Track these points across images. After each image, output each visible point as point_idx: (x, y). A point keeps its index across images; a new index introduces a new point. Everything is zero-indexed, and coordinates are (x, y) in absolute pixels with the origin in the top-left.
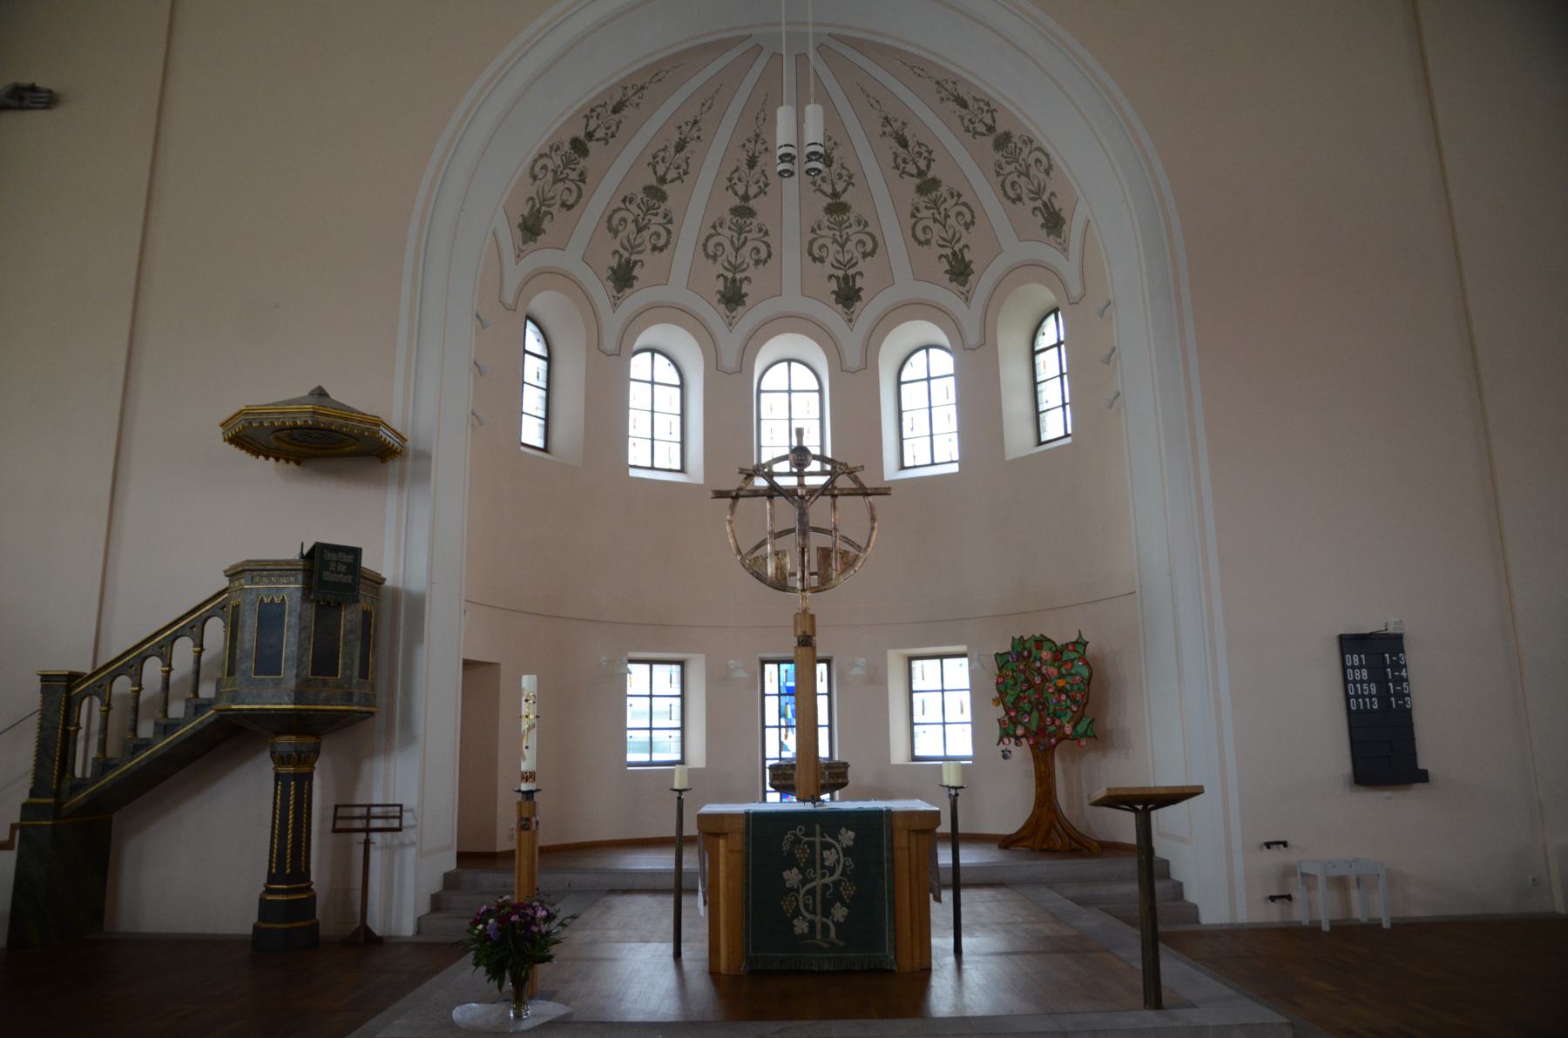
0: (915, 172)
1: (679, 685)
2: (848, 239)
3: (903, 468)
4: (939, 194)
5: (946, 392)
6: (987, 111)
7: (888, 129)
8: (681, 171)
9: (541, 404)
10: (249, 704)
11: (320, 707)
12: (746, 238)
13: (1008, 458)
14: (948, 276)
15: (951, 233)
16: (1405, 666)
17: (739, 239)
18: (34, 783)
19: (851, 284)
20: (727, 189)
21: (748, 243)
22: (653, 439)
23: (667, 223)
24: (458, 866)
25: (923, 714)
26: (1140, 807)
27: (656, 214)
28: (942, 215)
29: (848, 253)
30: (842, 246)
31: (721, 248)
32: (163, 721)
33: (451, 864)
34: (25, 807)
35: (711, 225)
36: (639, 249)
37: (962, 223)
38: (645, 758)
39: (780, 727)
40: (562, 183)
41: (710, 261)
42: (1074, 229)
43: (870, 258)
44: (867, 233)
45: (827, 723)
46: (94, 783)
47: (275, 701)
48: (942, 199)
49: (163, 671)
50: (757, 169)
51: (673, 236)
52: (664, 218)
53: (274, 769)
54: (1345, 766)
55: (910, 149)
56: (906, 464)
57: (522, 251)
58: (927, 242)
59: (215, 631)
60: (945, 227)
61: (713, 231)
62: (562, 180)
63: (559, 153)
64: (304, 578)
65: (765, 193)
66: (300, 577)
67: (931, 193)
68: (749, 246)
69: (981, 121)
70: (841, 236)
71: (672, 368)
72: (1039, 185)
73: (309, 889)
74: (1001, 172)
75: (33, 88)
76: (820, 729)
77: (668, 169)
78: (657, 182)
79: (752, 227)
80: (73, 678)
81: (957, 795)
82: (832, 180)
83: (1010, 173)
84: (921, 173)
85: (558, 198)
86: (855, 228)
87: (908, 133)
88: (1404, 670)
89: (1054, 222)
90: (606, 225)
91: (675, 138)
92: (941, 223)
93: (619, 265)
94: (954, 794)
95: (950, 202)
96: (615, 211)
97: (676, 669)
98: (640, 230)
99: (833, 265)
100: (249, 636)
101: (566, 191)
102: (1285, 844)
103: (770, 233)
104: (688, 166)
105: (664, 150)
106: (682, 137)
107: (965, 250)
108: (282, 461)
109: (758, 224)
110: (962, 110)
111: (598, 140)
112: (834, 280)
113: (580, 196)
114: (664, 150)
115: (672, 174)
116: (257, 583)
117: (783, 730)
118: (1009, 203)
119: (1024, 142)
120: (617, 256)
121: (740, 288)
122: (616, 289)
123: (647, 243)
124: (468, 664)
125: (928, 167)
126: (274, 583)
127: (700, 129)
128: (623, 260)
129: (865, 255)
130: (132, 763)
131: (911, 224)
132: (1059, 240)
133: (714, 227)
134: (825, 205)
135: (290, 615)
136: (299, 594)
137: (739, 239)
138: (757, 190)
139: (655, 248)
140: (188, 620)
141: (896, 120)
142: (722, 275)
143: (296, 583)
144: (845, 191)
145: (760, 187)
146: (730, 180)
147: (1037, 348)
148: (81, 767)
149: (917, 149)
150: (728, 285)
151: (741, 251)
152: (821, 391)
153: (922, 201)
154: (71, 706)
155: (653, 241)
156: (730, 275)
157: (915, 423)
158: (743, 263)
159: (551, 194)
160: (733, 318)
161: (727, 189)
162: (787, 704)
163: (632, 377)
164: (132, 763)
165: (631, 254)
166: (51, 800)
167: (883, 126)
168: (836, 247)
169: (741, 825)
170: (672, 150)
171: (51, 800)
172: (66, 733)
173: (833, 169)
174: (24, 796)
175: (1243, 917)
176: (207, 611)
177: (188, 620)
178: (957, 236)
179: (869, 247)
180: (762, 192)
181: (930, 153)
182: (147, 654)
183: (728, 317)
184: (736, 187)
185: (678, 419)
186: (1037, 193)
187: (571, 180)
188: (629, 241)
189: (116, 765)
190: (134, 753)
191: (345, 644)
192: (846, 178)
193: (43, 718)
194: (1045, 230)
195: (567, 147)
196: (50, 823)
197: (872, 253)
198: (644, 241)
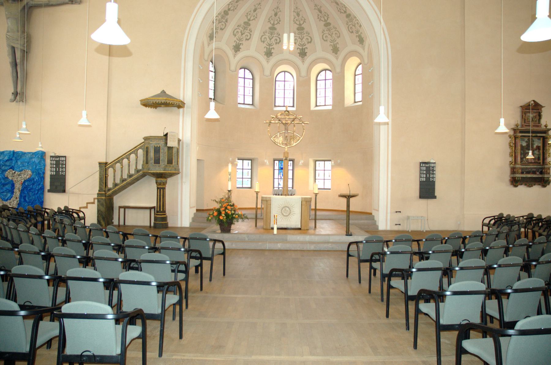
0: (324, 20)
1: (251, 166)
2: (303, 38)
4: (330, 27)
5: (329, 83)
6: (344, 7)
7: (316, 8)
9: (213, 86)
10: (153, 171)
11: (170, 172)
12: (273, 36)
13: (346, 106)
14: (332, 51)
15: (333, 39)
17: (271, 36)
19: (304, 51)
20: (268, 22)
22: (244, 95)
23: (250, 32)
24: (196, 212)
30: (302, 40)
32: (129, 175)
34: (98, 194)
36: (242, 40)
37: (337, 36)
39: (278, 179)
42: (366, 44)
44: (309, 36)
46: (113, 189)
47: (159, 170)
48: (331, 29)
54: (418, 194)
55: (322, 14)
56: (318, 105)
59: (140, 152)
60: (332, 37)
61: (264, 34)
63: (220, 15)
65: (279, 23)
66: (164, 140)
68: (274, 38)
72: (358, 30)
76: (289, 180)
77: (251, 17)
79: (275, 33)
80: (106, 163)
81: (317, 195)
84: (325, 21)
85: (220, 27)
86: (305, 35)
87: (322, 9)
89: (361, 41)
93: (236, 45)
95: (333, 30)
96: (235, 29)
97: (250, 162)
98: (242, 34)
99: (299, 45)
100: (152, 154)
101: (222, 25)
102: (400, 212)
103: (280, 35)
104: (257, 16)
106: (256, 8)
110: (337, 6)
111: (232, 10)
112: (299, 49)
113: (225, 26)
115: (252, 18)
117: (279, 180)
119: (354, 17)
121: (271, 51)
124: (197, 160)
125: (328, 19)
127: (261, 6)
128: (237, 43)
129: (308, 43)
130: (122, 184)
131: (322, 35)
132: (362, 46)
133: (264, 33)
136: (164, 145)
137: (271, 36)
140: (134, 150)
141: (318, 5)
142: (266, 47)
145: (278, 22)
148: (110, 185)
151: (271, 40)
154: (106, 170)
155: (246, 37)
156: (268, 47)
158: (272, 43)
161: (268, 22)
163: (289, 178)
164: (122, 184)
166: (104, 193)
168: (300, 40)
170: (252, 11)
172: (106, 177)
174: (97, 192)
175: (389, 228)
177: (134, 150)
179: (310, 40)
180: (278, 23)
181: (328, 15)
183: (267, 59)
184: (271, 21)
185: (252, 89)
186: (357, 32)
188: (239, 38)
189: (119, 185)
190: (122, 182)
192: (303, 20)
193: (100, 173)
195: (223, 13)
197: (310, 42)
198: (243, 38)
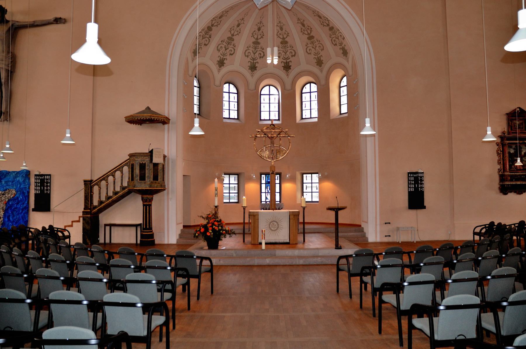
1: (237, 181)
2: (287, 51)
3: (302, 119)
8: (238, 32)
10: (139, 188)
11: (155, 188)
12: (257, 50)
15: (317, 52)
16: (423, 180)
18: (85, 206)
20: (252, 37)
21: (257, 52)
25: (306, 189)
26: (336, 210)
27: (231, 45)
28: (315, 46)
29: (287, 55)
30: (286, 53)
31: (250, 53)
32: (115, 192)
33: (182, 228)
34: (83, 212)
35: (247, 47)
37: (320, 49)
38: (228, 201)
40: (204, 39)
41: (247, 57)
42: (350, 56)
43: (294, 57)
45: (279, 192)
47: (145, 187)
49: (113, 180)
50: (261, 31)
51: (235, 50)
52: (233, 45)
53: (143, 203)
56: (303, 117)
57: (193, 59)
58: (310, 53)
59: (126, 169)
62: (204, 38)
64: (150, 157)
66: (149, 157)
67: (311, 40)
68: (258, 52)
69: (325, 22)
70: (285, 50)
71: (235, 88)
73: (152, 232)
74: (331, 37)
75: (60, 18)
78: (231, 36)
81: (305, 208)
82: (283, 34)
83: (333, 37)
84: (308, 34)
86: (289, 48)
87: (305, 23)
88: (423, 181)
89: (345, 53)
90: (217, 49)
91: (237, 23)
92: (314, 48)
93: (220, 60)
94: (304, 208)
95: (317, 43)
96: (219, 45)
100: (137, 171)
102: (390, 223)
105: (233, 27)
107: (321, 57)
108: (134, 124)
109: (261, 46)
110: (320, 19)
114: (233, 27)
116: (138, 159)
117: (267, 194)
118: (333, 45)
119: (337, 30)
120: (219, 57)
122: (219, 67)
123: (228, 53)
125: (311, 32)
126: (143, 158)
129: (292, 56)
132: (346, 58)
134: (280, 41)
135: (147, 166)
136: (149, 161)
137: (255, 51)
138: (261, 37)
139: (230, 54)
142: (250, 61)
143: (148, 158)
144: (287, 37)
146: (252, 34)
147: (341, 86)
148: (95, 203)
149: (307, 27)
150: (252, 64)
152: (279, 95)
153: (309, 41)
154: (92, 188)
157: (306, 105)
159: (201, 42)
160: (253, 74)
161: (252, 37)
162: (268, 186)
165: (223, 56)
167: (298, 20)
169: (54, 326)
170: (236, 27)
171: (89, 211)
173: (283, 31)
174: (83, 210)
176: (124, 164)
178: (319, 52)
179: (293, 54)
180: (262, 37)
182: (109, 175)
183: (251, 74)
186: (341, 44)
187: (207, 38)
188: (223, 53)
191: (160, 173)
193: (85, 191)
194: (343, 55)
196: (90, 216)
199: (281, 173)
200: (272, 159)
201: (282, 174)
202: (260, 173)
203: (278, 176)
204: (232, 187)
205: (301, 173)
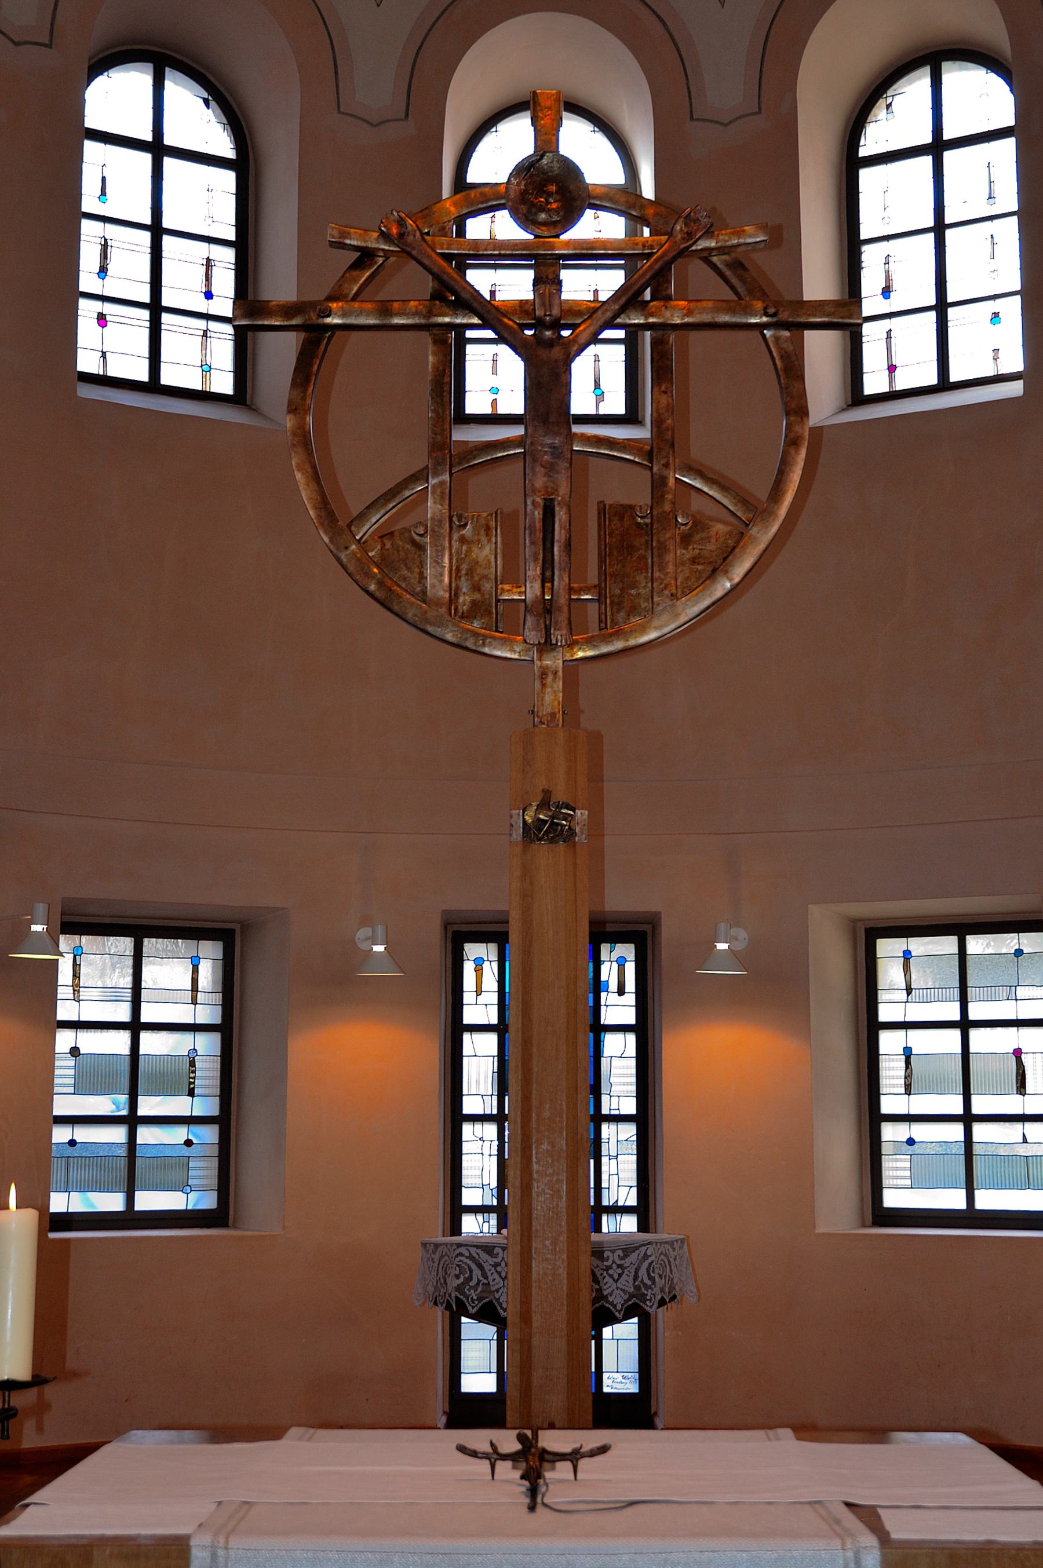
1: (218, 998)
3: (857, 398)
199: (653, 921)
200: (533, 636)
201: (668, 931)
202: (446, 925)
203: (627, 951)
204: (935, 1088)
205: (854, 923)
